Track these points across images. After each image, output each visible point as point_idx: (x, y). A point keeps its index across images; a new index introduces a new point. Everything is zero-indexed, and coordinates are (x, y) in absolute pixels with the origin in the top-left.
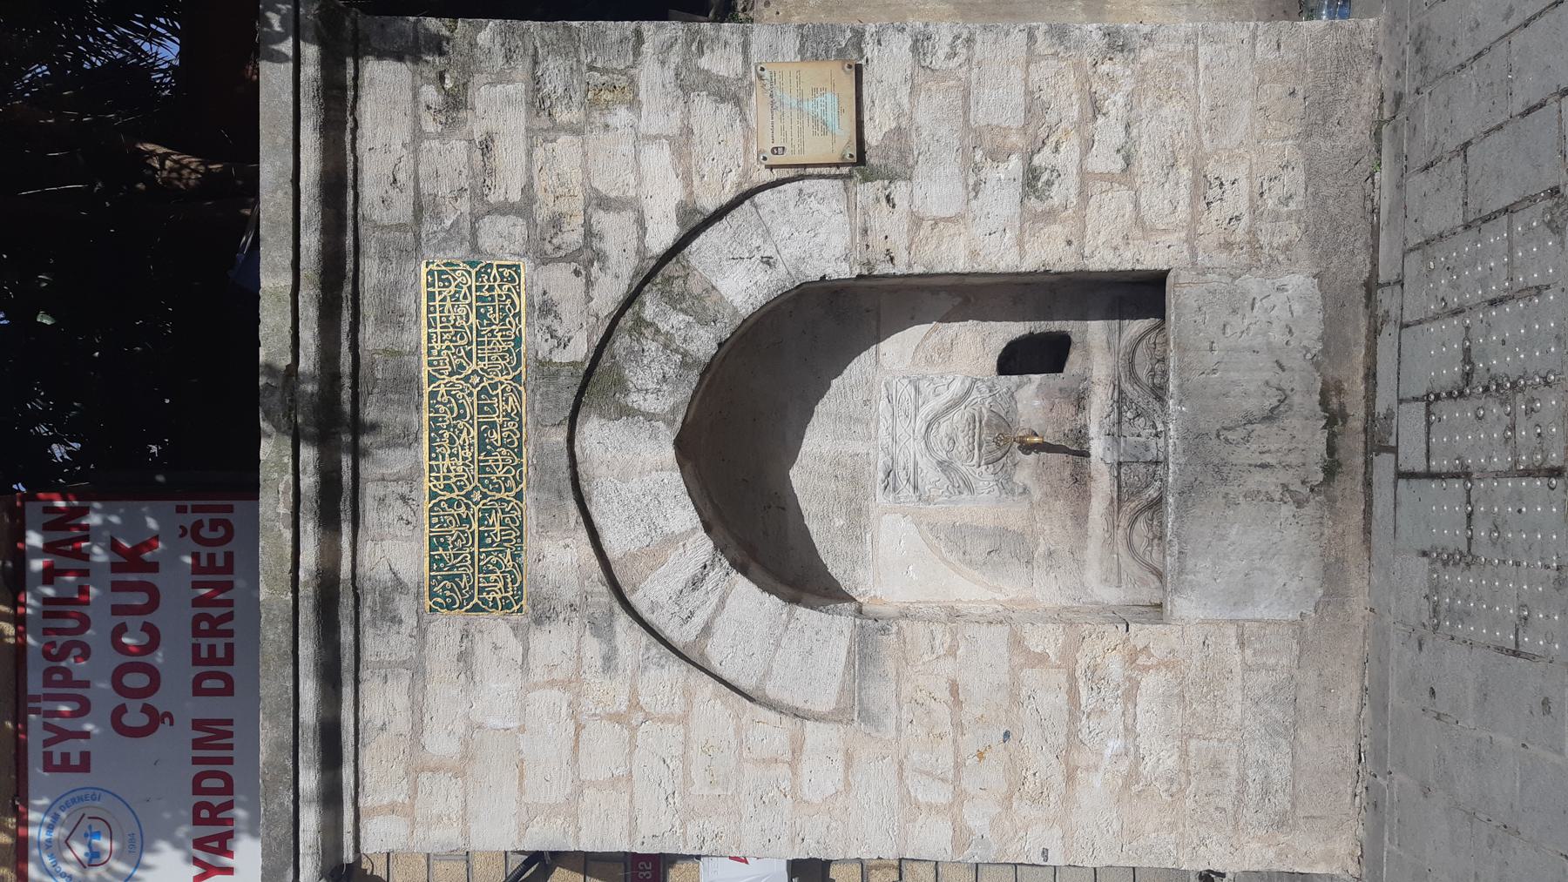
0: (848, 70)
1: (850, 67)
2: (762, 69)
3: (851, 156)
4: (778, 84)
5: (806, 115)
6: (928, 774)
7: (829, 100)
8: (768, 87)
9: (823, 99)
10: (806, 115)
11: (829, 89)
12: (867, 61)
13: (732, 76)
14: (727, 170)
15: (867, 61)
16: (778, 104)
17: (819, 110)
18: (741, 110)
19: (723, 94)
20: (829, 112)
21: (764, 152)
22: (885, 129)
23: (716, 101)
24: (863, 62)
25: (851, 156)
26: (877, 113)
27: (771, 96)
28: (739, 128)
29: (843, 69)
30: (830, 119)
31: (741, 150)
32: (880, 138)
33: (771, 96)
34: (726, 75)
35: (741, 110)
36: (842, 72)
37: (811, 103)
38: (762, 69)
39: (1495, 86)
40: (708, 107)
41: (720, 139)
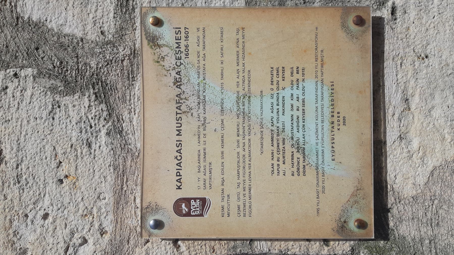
0: (352, 27)
1: (360, 22)
2: (158, 23)
3: (362, 225)
4: (193, 57)
5: (256, 129)
6: (121, 226)
7: (310, 97)
8: (170, 61)
9: (296, 92)
10: (256, 129)
11: (310, 67)
12: (393, 11)
13: (92, 35)
14: (76, 240)
15: (393, 11)
16: (192, 102)
17: (286, 119)
18: (111, 111)
19: (71, 74)
20: (311, 124)
21: (157, 209)
22: (431, 163)
23: (53, 89)
24: (385, 13)
25: (362, 225)
26: (417, 125)
27: (178, 83)
28: (105, 150)
29: (344, 26)
30: (311, 139)
31: (109, 197)
32: (421, 180)
33: (178, 83)
34: (79, 34)
35: (111, 111)
36: (341, 34)
37: (267, 101)
38: (158, 23)
39: (30, 168)
40: (36, 104)
41: (61, 173)
